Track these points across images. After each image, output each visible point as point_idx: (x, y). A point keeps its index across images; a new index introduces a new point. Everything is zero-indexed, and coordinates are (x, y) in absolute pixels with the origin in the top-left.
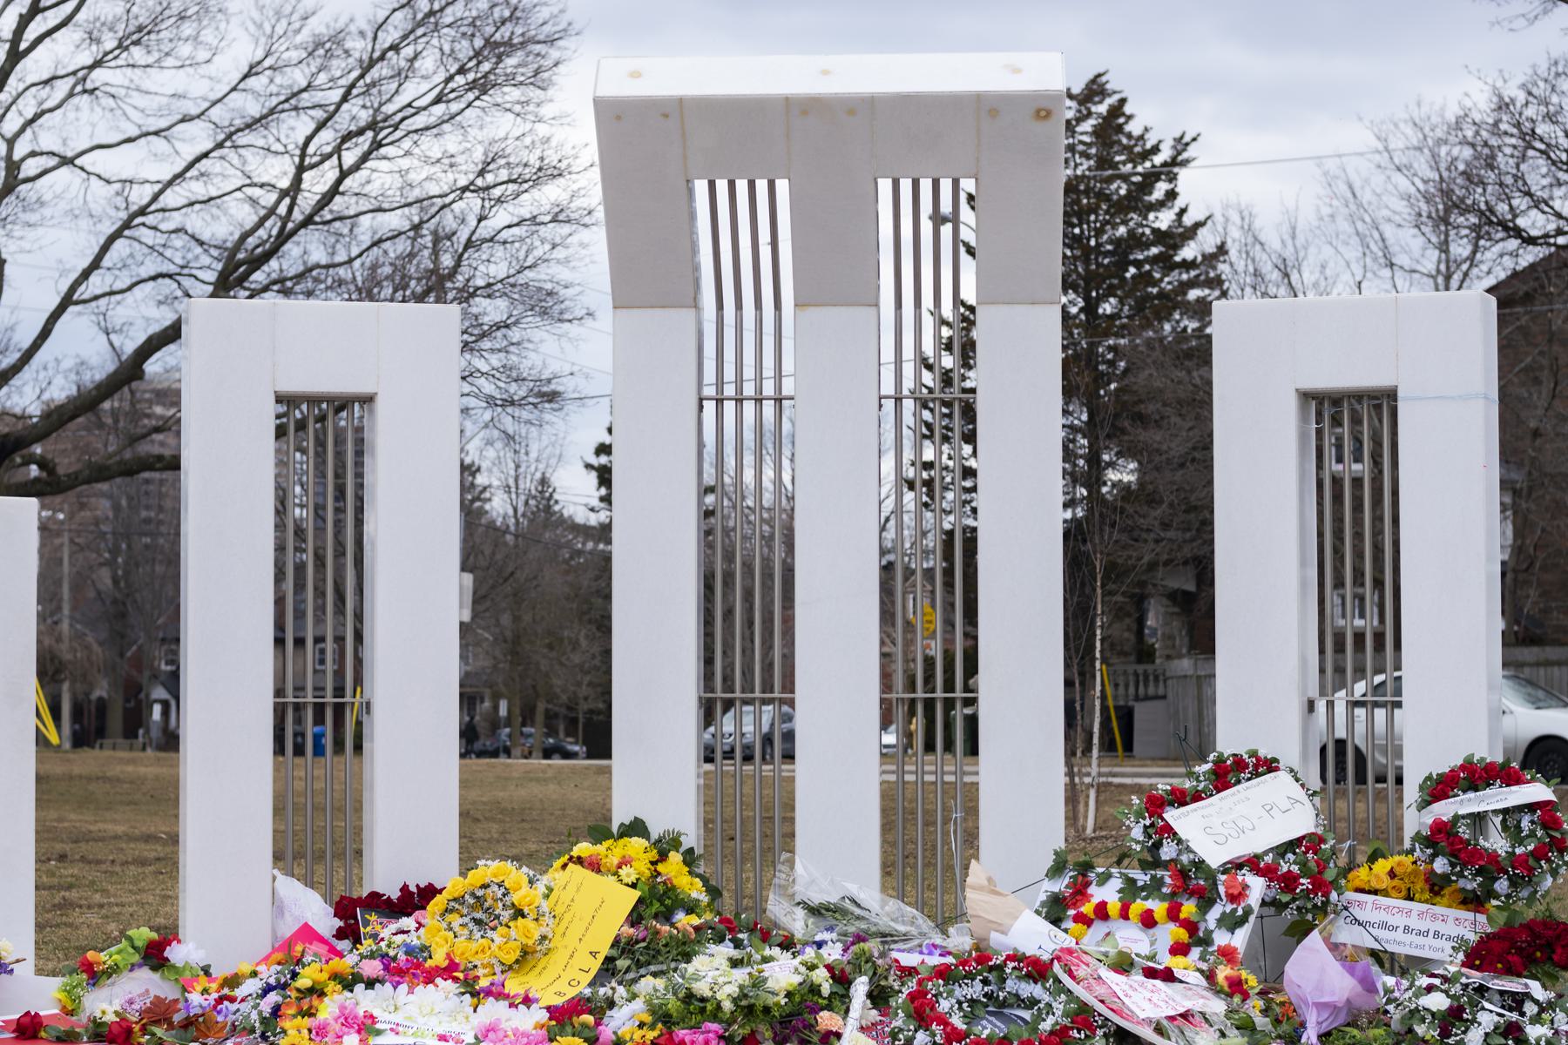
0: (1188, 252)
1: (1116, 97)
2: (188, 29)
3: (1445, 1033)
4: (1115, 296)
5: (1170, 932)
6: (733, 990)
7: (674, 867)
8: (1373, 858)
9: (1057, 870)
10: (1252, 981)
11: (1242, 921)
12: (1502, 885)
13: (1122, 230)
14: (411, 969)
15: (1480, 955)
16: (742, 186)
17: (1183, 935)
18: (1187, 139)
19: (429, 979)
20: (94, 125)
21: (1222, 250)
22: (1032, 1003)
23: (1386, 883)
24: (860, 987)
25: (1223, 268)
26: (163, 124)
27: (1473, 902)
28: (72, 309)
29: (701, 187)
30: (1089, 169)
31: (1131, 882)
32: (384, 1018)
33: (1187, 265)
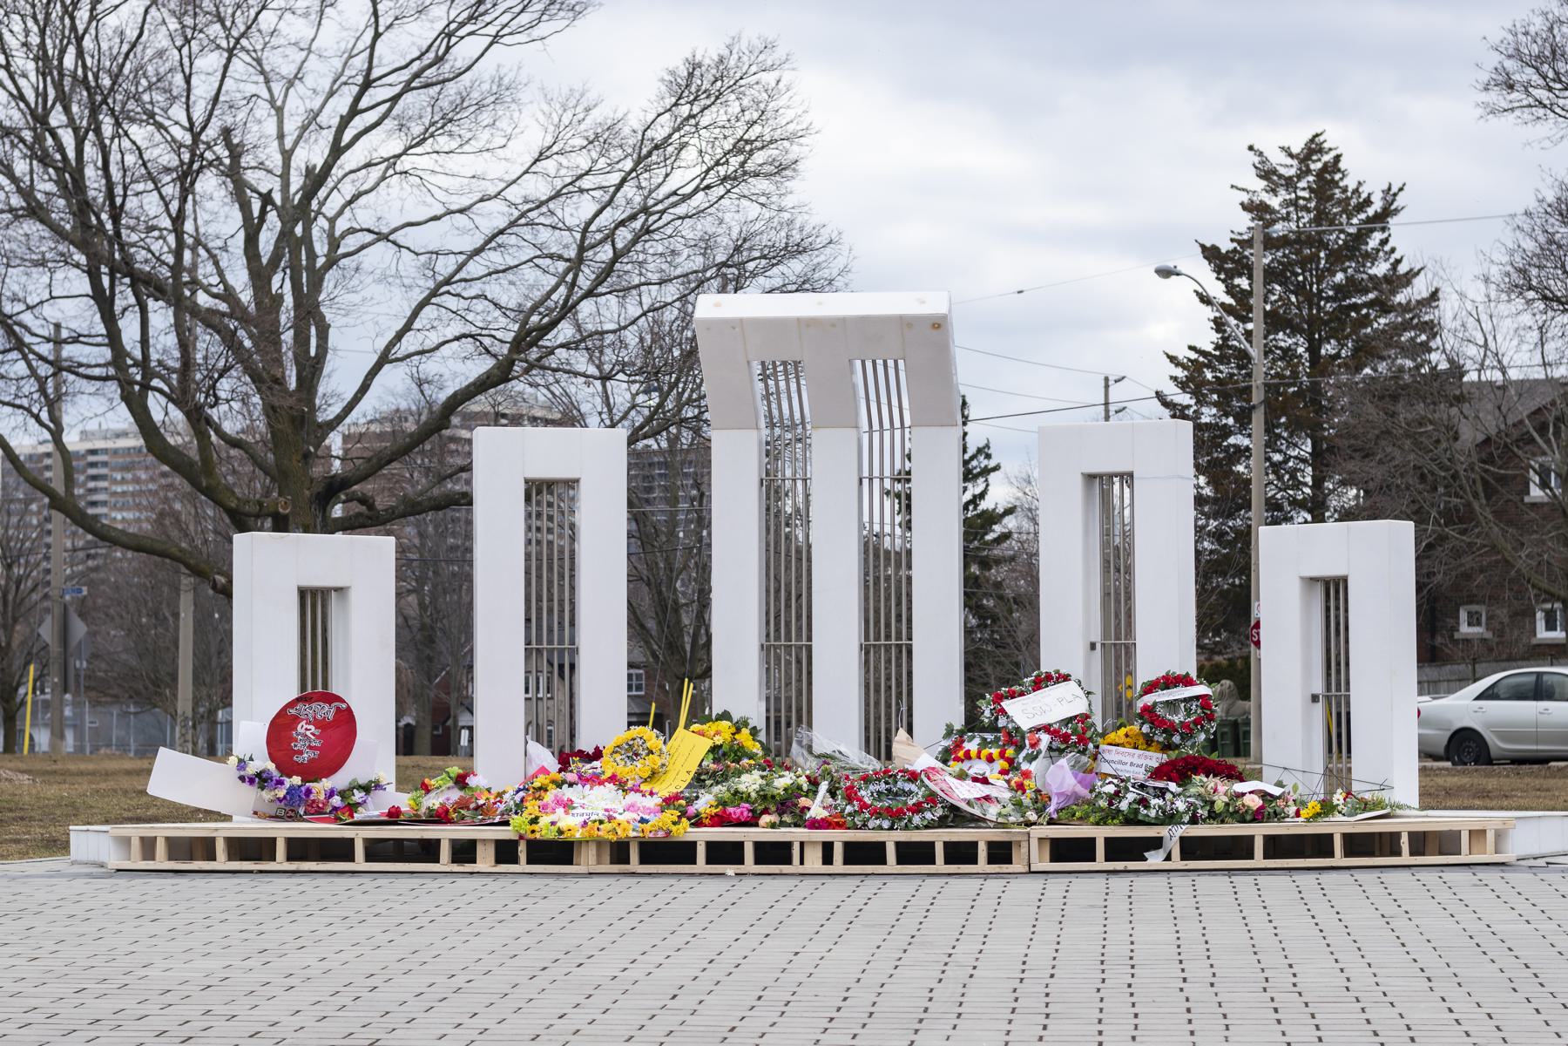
1: (1333, 154)
2: (486, 118)
6: (756, 787)
7: (744, 737)
11: (1035, 758)
12: (1176, 739)
13: (1340, 277)
14: (595, 780)
15: (1157, 773)
17: (1006, 765)
19: (601, 783)
21: (1434, 296)
22: (911, 792)
26: (465, 202)
27: (1166, 747)
28: (387, 367)
30: (1310, 222)
31: (984, 740)
32: (577, 801)
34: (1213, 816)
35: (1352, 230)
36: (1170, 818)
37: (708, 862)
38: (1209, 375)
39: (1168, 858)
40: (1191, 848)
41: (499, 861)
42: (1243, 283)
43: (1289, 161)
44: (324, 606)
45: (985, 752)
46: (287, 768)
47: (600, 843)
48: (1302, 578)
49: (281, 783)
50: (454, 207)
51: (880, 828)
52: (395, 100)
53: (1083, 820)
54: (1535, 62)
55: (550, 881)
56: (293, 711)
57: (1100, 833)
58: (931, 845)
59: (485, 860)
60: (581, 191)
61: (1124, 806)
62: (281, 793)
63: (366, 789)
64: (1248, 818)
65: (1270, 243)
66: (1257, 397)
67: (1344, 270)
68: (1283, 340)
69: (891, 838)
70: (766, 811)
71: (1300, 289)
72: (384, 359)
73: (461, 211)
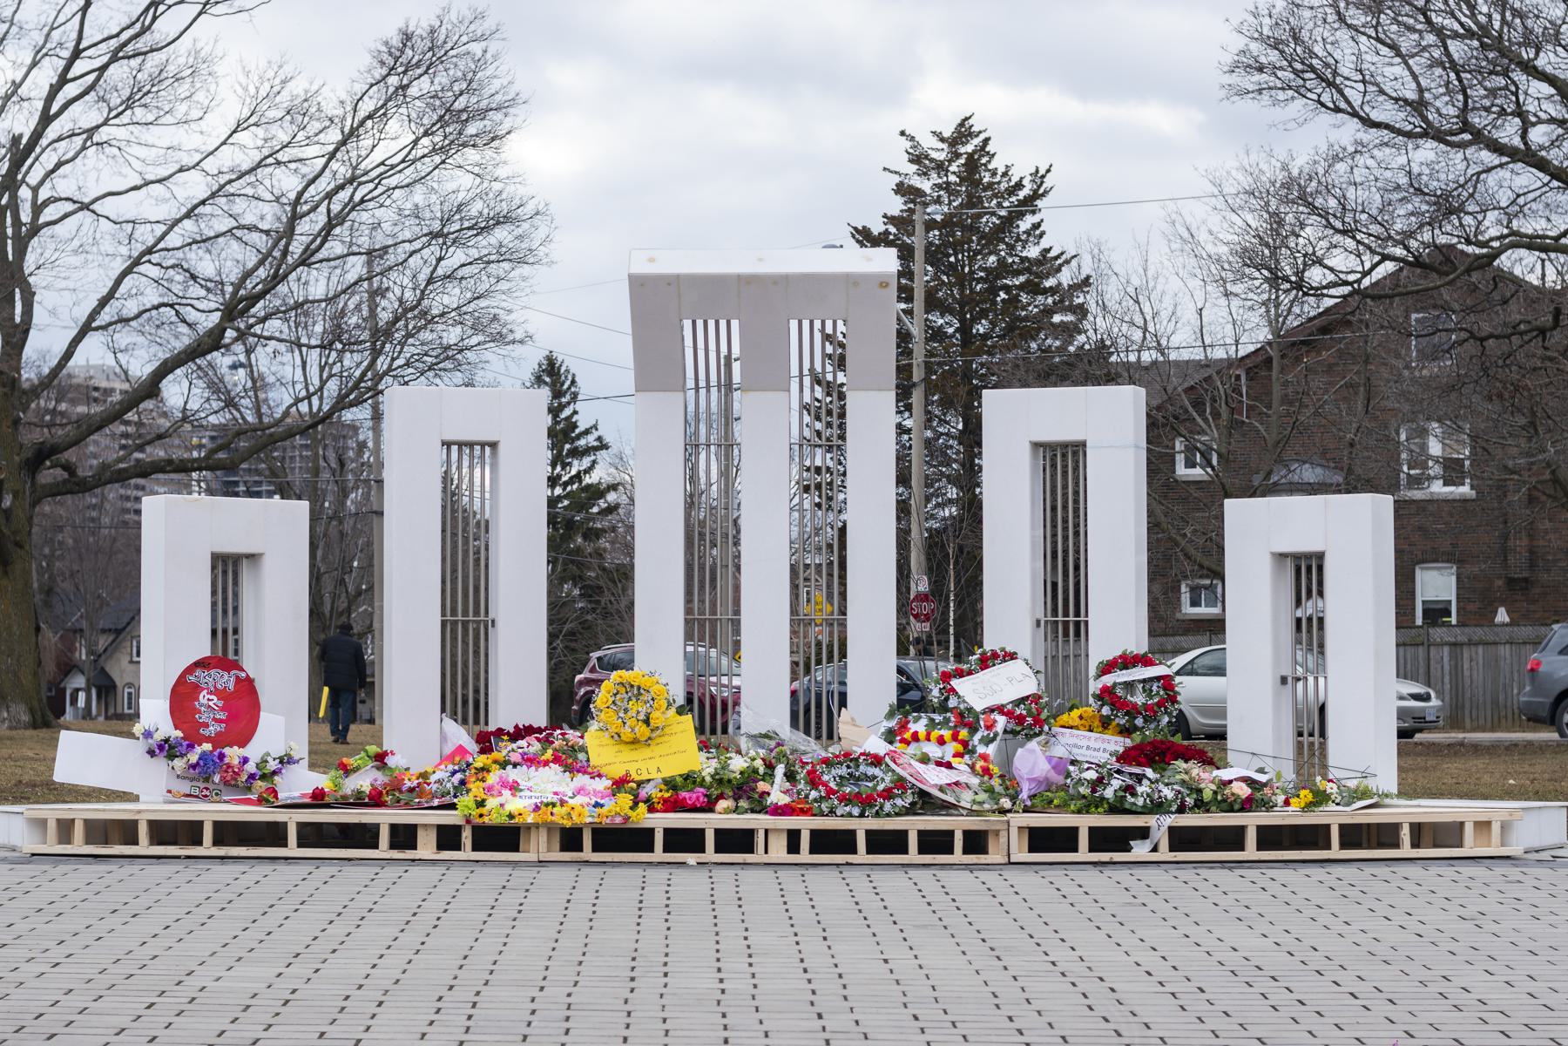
1: (982, 137)
2: (183, 89)
3: (1094, 791)
4: (986, 318)
5: (952, 747)
6: (711, 770)
8: (1071, 709)
9: (890, 715)
10: (995, 770)
15: (1126, 757)
16: (711, 323)
17: (960, 748)
20: (99, 171)
24: (780, 770)
27: (1125, 731)
29: (687, 324)
31: (932, 720)
34: (1201, 805)
35: (1003, 213)
36: (1158, 807)
39: (1155, 849)
40: (1182, 839)
43: (941, 145)
45: (935, 734)
47: (550, 828)
48: (1273, 554)
50: (152, 178)
51: (850, 815)
53: (1062, 807)
54: (1276, 45)
55: (266, 868)
56: (192, 678)
57: (1084, 823)
58: (904, 833)
59: (426, 847)
60: (278, 163)
61: (1109, 793)
64: (1237, 807)
65: (930, 225)
69: (861, 826)
70: (721, 797)
72: (86, 329)
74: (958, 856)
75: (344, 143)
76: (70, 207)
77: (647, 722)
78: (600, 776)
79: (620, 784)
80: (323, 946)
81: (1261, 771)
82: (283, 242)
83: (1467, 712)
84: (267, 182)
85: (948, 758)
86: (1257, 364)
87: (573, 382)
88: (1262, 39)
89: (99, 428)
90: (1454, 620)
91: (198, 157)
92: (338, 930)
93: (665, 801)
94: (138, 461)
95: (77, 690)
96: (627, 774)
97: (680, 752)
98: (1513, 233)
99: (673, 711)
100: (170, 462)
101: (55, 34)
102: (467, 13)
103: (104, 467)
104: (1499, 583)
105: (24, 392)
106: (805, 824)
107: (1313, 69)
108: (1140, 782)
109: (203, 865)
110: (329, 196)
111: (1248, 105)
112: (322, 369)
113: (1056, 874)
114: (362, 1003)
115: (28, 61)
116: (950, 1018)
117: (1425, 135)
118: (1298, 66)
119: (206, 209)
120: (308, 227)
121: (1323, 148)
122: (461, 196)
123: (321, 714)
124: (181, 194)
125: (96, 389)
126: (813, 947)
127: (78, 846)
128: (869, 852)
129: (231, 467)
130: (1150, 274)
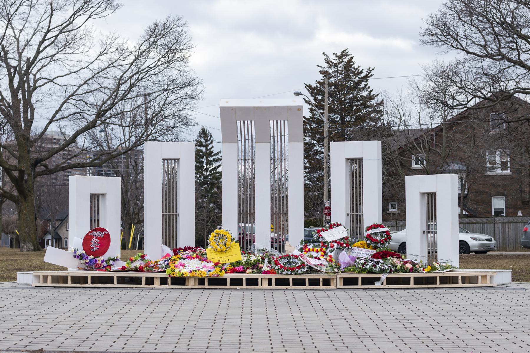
0: (373, 102)
2: (82, 42)
5: (321, 253)
6: (245, 260)
9: (302, 243)
10: (333, 260)
11: (333, 251)
12: (379, 245)
13: (351, 96)
15: (374, 256)
17: (323, 253)
18: (371, 69)
21: (382, 102)
22: (295, 262)
23: (360, 245)
24: (266, 260)
25: (381, 108)
26: (76, 69)
27: (375, 248)
30: (342, 78)
31: (314, 245)
32: (187, 265)
33: (371, 106)
34: (396, 271)
35: (356, 81)
36: (383, 271)
37: (246, 285)
38: (308, 127)
39: (382, 284)
40: (390, 281)
41: (161, 284)
42: (320, 97)
43: (336, 58)
44: (98, 201)
45: (315, 249)
46: (89, 253)
47: (195, 278)
49: (88, 258)
52: (57, 36)
53: (354, 271)
54: (438, 26)
55: (107, 290)
57: (360, 276)
61: (368, 267)
62: (87, 261)
63: (113, 260)
65: (330, 85)
66: (326, 134)
67: (353, 94)
68: (333, 116)
69: (291, 277)
70: (248, 268)
71: (339, 99)
72: (51, 121)
73: (75, 72)
74: (321, 286)
75: (135, 60)
76: (46, 81)
77: (225, 245)
78: (210, 262)
79: (216, 264)
80: (123, 312)
81: (416, 260)
82: (116, 93)
83: (507, 245)
84: (111, 73)
85: (319, 256)
86: (439, 130)
87: (211, 136)
88: (433, 25)
89: (56, 153)
90: (504, 215)
91: (88, 64)
92: (128, 307)
93: (231, 270)
94: (69, 163)
95: (49, 240)
96: (219, 261)
97: (235, 255)
98: (518, 88)
99: (234, 242)
100: (79, 164)
101: (41, 25)
102: (176, 18)
103: (57, 166)
104: (519, 202)
105: (31, 142)
106: (274, 277)
107: (449, 35)
108: (378, 264)
109: (88, 289)
110: (131, 77)
111: (429, 46)
112: (130, 133)
113: (351, 292)
114: (134, 327)
115: (32, 33)
116: (308, 330)
117: (486, 56)
118: (445, 34)
119: (91, 81)
120: (124, 88)
121: (454, 61)
122: (174, 77)
123: (129, 247)
124: (82, 76)
125: (55, 139)
126: (271, 312)
127: (49, 284)
128: (293, 285)
129: (100, 165)
130: (402, 101)
